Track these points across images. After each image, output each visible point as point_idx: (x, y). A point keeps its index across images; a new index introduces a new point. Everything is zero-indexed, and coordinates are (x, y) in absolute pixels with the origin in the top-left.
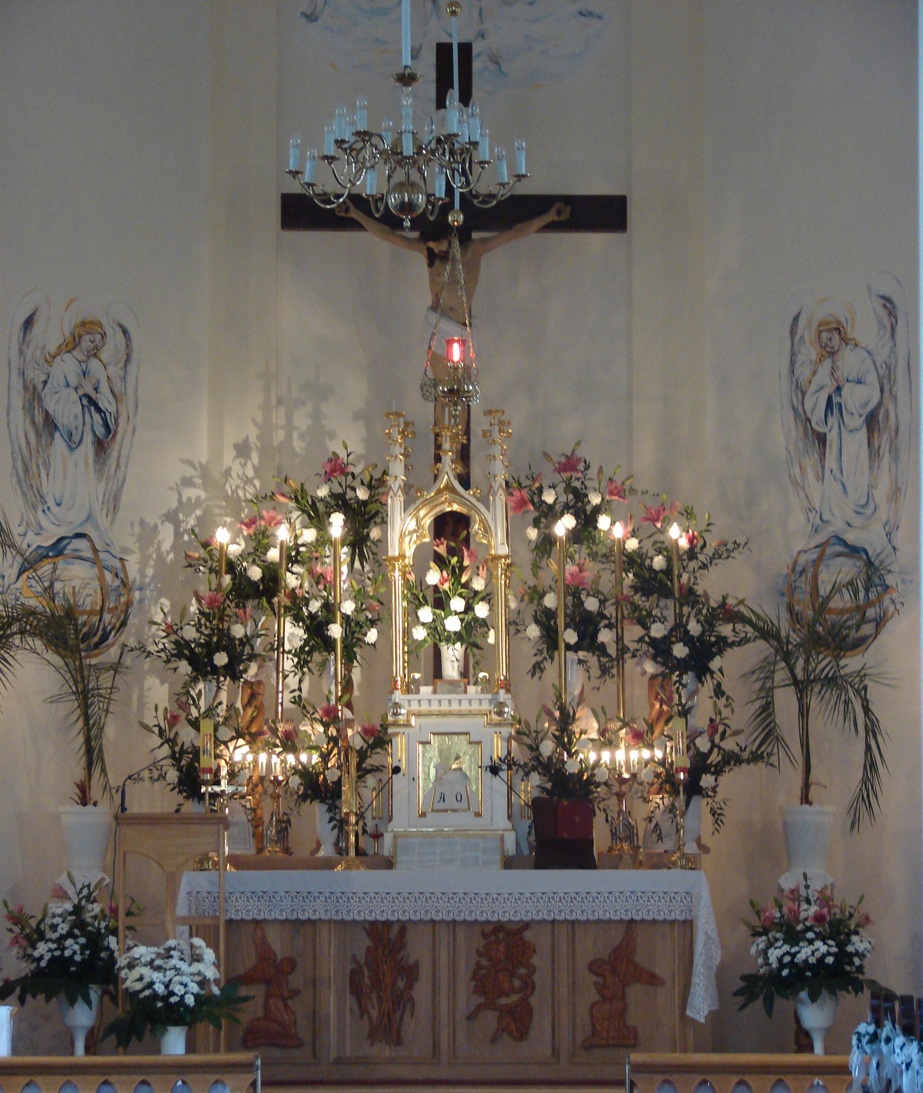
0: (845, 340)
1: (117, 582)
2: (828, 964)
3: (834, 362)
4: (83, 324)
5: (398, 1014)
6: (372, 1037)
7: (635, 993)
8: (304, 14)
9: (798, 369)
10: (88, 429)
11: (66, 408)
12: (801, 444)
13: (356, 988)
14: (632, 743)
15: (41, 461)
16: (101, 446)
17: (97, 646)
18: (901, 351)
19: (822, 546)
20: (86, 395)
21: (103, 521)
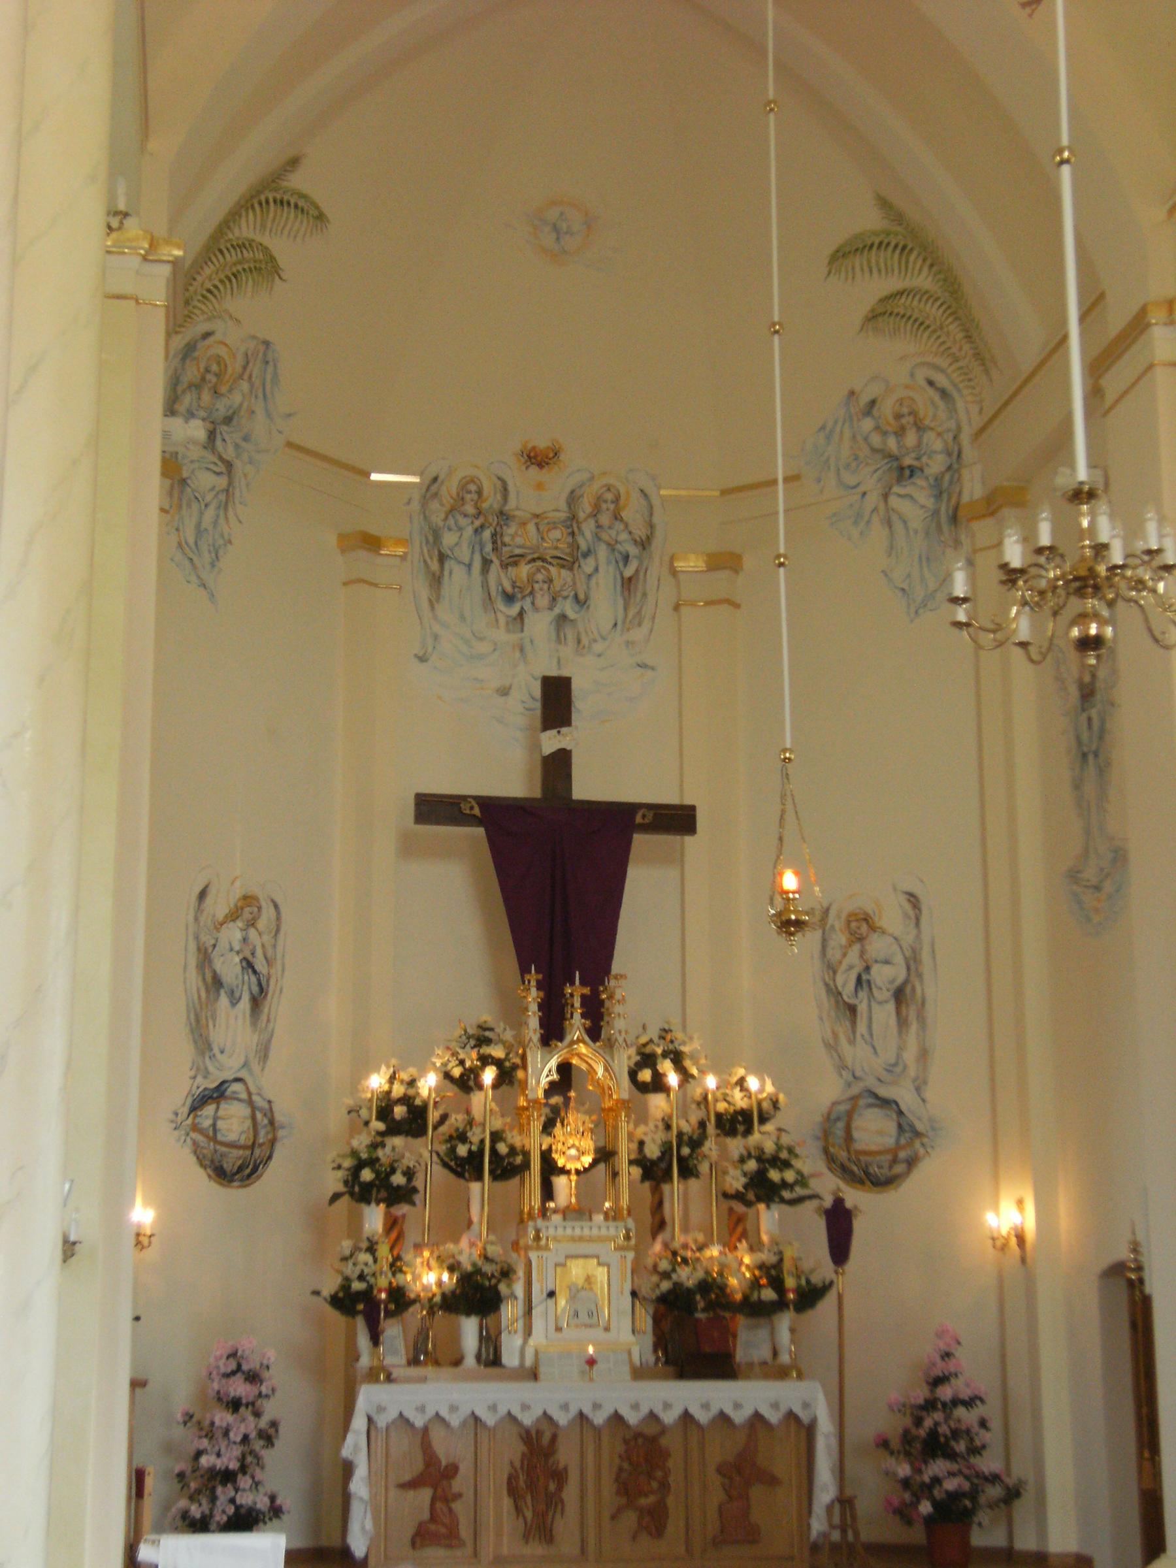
0: (873, 928)
1: (266, 1121)
3: (863, 946)
4: (245, 898)
5: (551, 1514)
6: (526, 1537)
7: (757, 1492)
8: (416, 656)
9: (829, 952)
10: (246, 987)
11: (229, 968)
12: (833, 1014)
13: (513, 1491)
15: (209, 1014)
16: (256, 1003)
17: (249, 1176)
18: (926, 939)
19: (854, 1099)
20: (245, 959)
21: (256, 1068)
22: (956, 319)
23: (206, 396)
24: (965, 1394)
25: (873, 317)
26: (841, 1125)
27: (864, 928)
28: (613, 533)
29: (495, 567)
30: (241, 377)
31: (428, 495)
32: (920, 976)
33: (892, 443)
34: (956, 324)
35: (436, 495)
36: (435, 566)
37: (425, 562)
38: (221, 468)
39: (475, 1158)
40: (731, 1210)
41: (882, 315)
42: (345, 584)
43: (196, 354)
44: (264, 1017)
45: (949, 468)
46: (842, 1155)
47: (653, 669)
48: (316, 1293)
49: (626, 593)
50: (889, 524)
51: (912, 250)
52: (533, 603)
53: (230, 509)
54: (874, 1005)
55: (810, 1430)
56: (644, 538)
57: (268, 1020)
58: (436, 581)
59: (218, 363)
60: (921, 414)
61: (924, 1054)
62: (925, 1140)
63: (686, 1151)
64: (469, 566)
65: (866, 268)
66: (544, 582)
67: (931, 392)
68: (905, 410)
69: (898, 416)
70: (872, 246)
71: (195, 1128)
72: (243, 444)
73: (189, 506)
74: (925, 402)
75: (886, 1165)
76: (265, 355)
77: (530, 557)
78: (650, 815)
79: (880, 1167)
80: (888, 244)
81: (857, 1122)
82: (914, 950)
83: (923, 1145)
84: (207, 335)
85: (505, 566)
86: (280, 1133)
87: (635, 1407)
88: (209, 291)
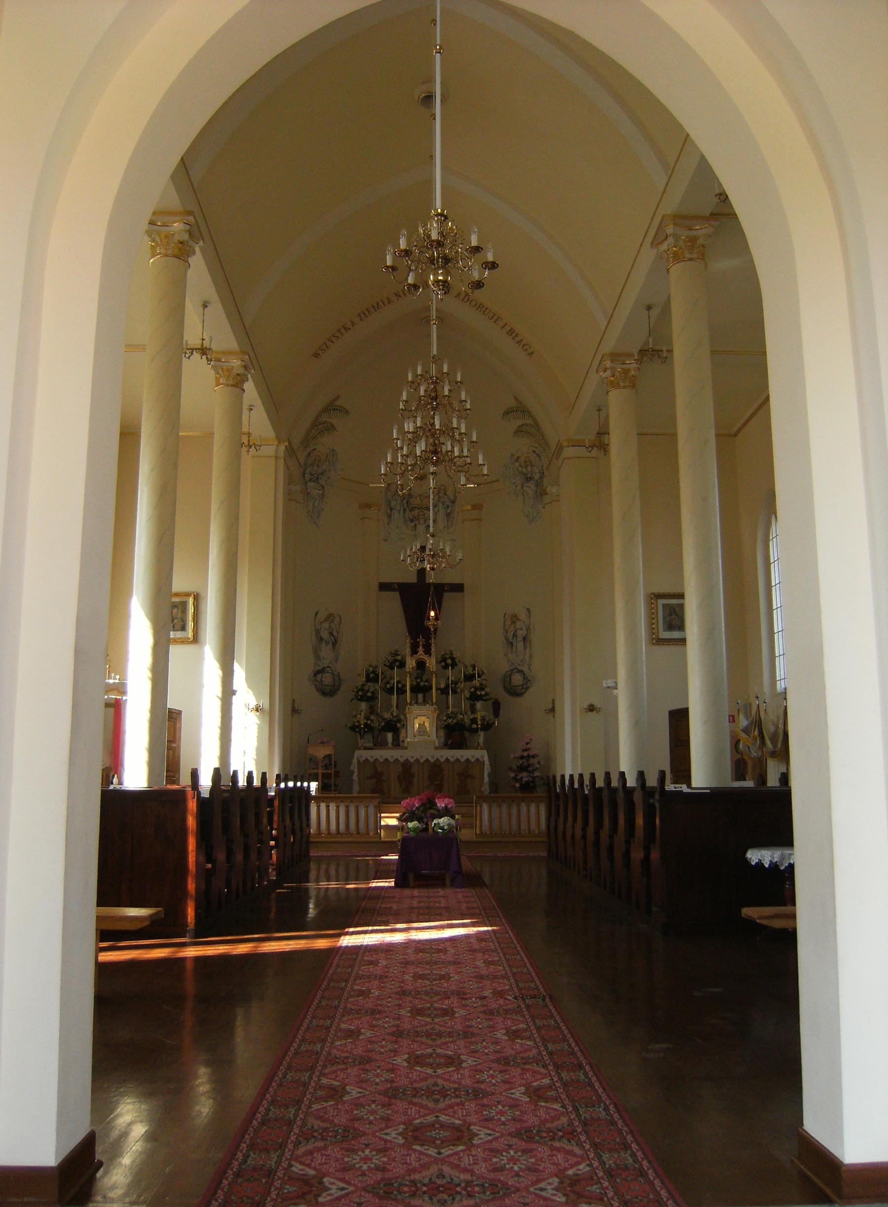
2: (746, 862)
11: (325, 635)
13: (399, 780)
14: (99, 1198)
16: (334, 644)
23: (315, 468)
24: (531, 753)
41: (518, 432)
61: (531, 657)
71: (315, 680)
81: (513, 677)
87: (433, 757)
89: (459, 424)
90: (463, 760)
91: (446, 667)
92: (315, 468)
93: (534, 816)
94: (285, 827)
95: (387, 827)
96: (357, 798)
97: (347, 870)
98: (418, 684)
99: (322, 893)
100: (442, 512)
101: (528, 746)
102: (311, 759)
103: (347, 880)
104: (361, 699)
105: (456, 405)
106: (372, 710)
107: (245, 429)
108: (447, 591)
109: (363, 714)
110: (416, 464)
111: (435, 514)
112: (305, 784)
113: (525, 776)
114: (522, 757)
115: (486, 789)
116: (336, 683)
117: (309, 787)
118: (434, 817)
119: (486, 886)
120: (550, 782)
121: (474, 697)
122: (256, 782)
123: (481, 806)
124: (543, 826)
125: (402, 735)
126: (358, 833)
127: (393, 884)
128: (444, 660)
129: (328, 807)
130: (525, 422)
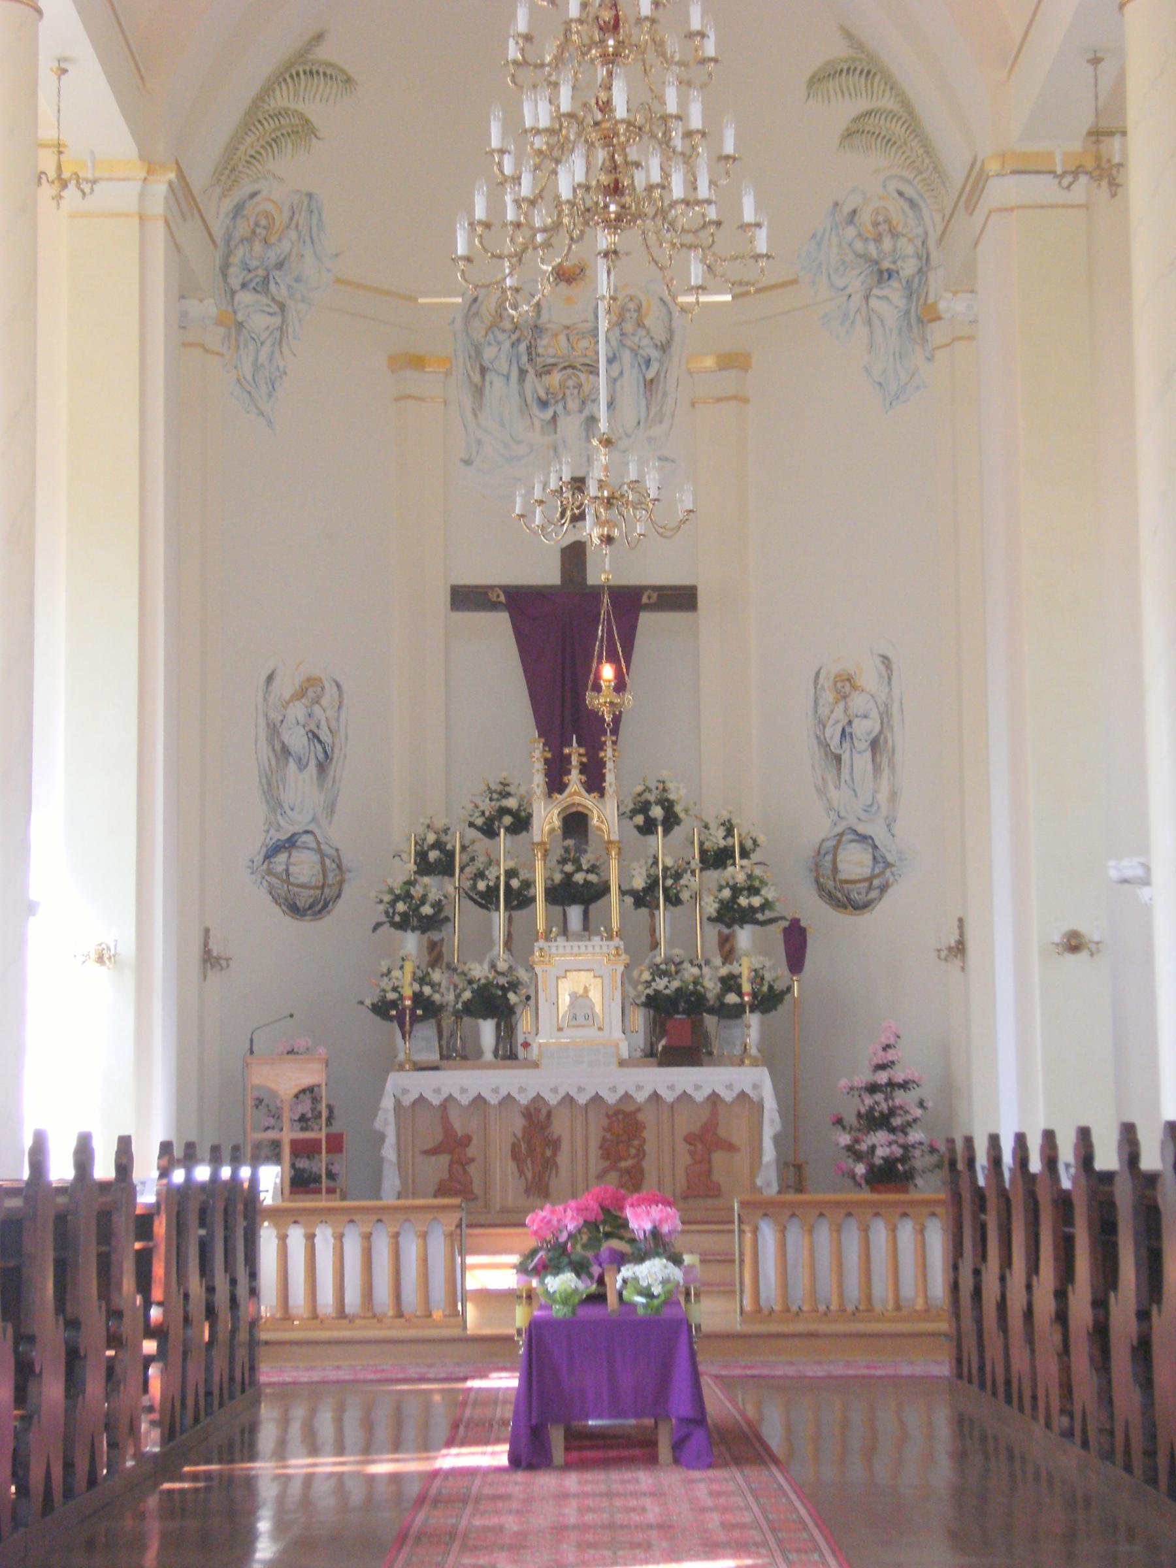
0: (854, 687)
1: (334, 866)
4: (309, 680)
10: (312, 754)
11: (297, 740)
13: (515, 1156)
16: (322, 768)
19: (841, 835)
22: (916, 136)
23: (258, 247)
24: (899, 1077)
25: (848, 135)
26: (829, 858)
27: (847, 688)
28: (636, 339)
29: (531, 375)
30: (288, 227)
31: (471, 313)
32: (891, 728)
33: (872, 248)
34: (916, 141)
35: (476, 314)
36: (477, 378)
37: (469, 375)
38: (275, 308)
39: (492, 892)
40: (720, 933)
41: (853, 133)
42: (397, 400)
43: (245, 213)
44: (330, 778)
45: (920, 270)
46: (830, 884)
47: (673, 461)
48: (361, 1003)
49: (648, 393)
50: (869, 322)
51: (875, 74)
52: (565, 408)
53: (284, 344)
54: (855, 755)
55: (759, 1107)
56: (664, 342)
57: (334, 782)
58: (479, 392)
59: (266, 217)
60: (894, 223)
61: (894, 796)
62: (894, 869)
63: (669, 882)
64: (507, 377)
65: (838, 90)
66: (574, 387)
67: (901, 202)
68: (881, 219)
69: (876, 224)
70: (842, 71)
71: (270, 872)
72: (295, 285)
73: (246, 345)
74: (896, 209)
75: (863, 891)
76: (309, 205)
77: (561, 366)
78: (655, 595)
79: (859, 894)
80: (855, 69)
81: (841, 856)
82: (886, 706)
83: (893, 874)
84: (253, 195)
85: (539, 375)
86: (347, 876)
88: (252, 157)
89: (683, 103)
90: (699, 1096)
91: (648, 828)
92: (258, 247)
93: (911, 1258)
94: (186, 1296)
95: (486, 1296)
96: (396, 1209)
97: (368, 1425)
98: (569, 876)
99: (295, 1488)
100: (630, 383)
101: (891, 1055)
102: (259, 1102)
103: (368, 1450)
104: (403, 924)
105: (673, 46)
106: (435, 954)
107: (47, 132)
108: (650, 607)
109: (409, 967)
110: (558, 225)
111: (613, 381)
112: (245, 1172)
113: (881, 1144)
114: (873, 1088)
115: (768, 1180)
116: (331, 879)
117: (254, 1180)
118: (620, 1260)
119: (775, 1460)
120: (955, 1162)
121: (731, 914)
122: (104, 1169)
123: (755, 1230)
124: (938, 1287)
125: (524, 1023)
126: (400, 1314)
127: (504, 1461)
128: (643, 808)
129: (310, 1238)
130: (875, 104)
